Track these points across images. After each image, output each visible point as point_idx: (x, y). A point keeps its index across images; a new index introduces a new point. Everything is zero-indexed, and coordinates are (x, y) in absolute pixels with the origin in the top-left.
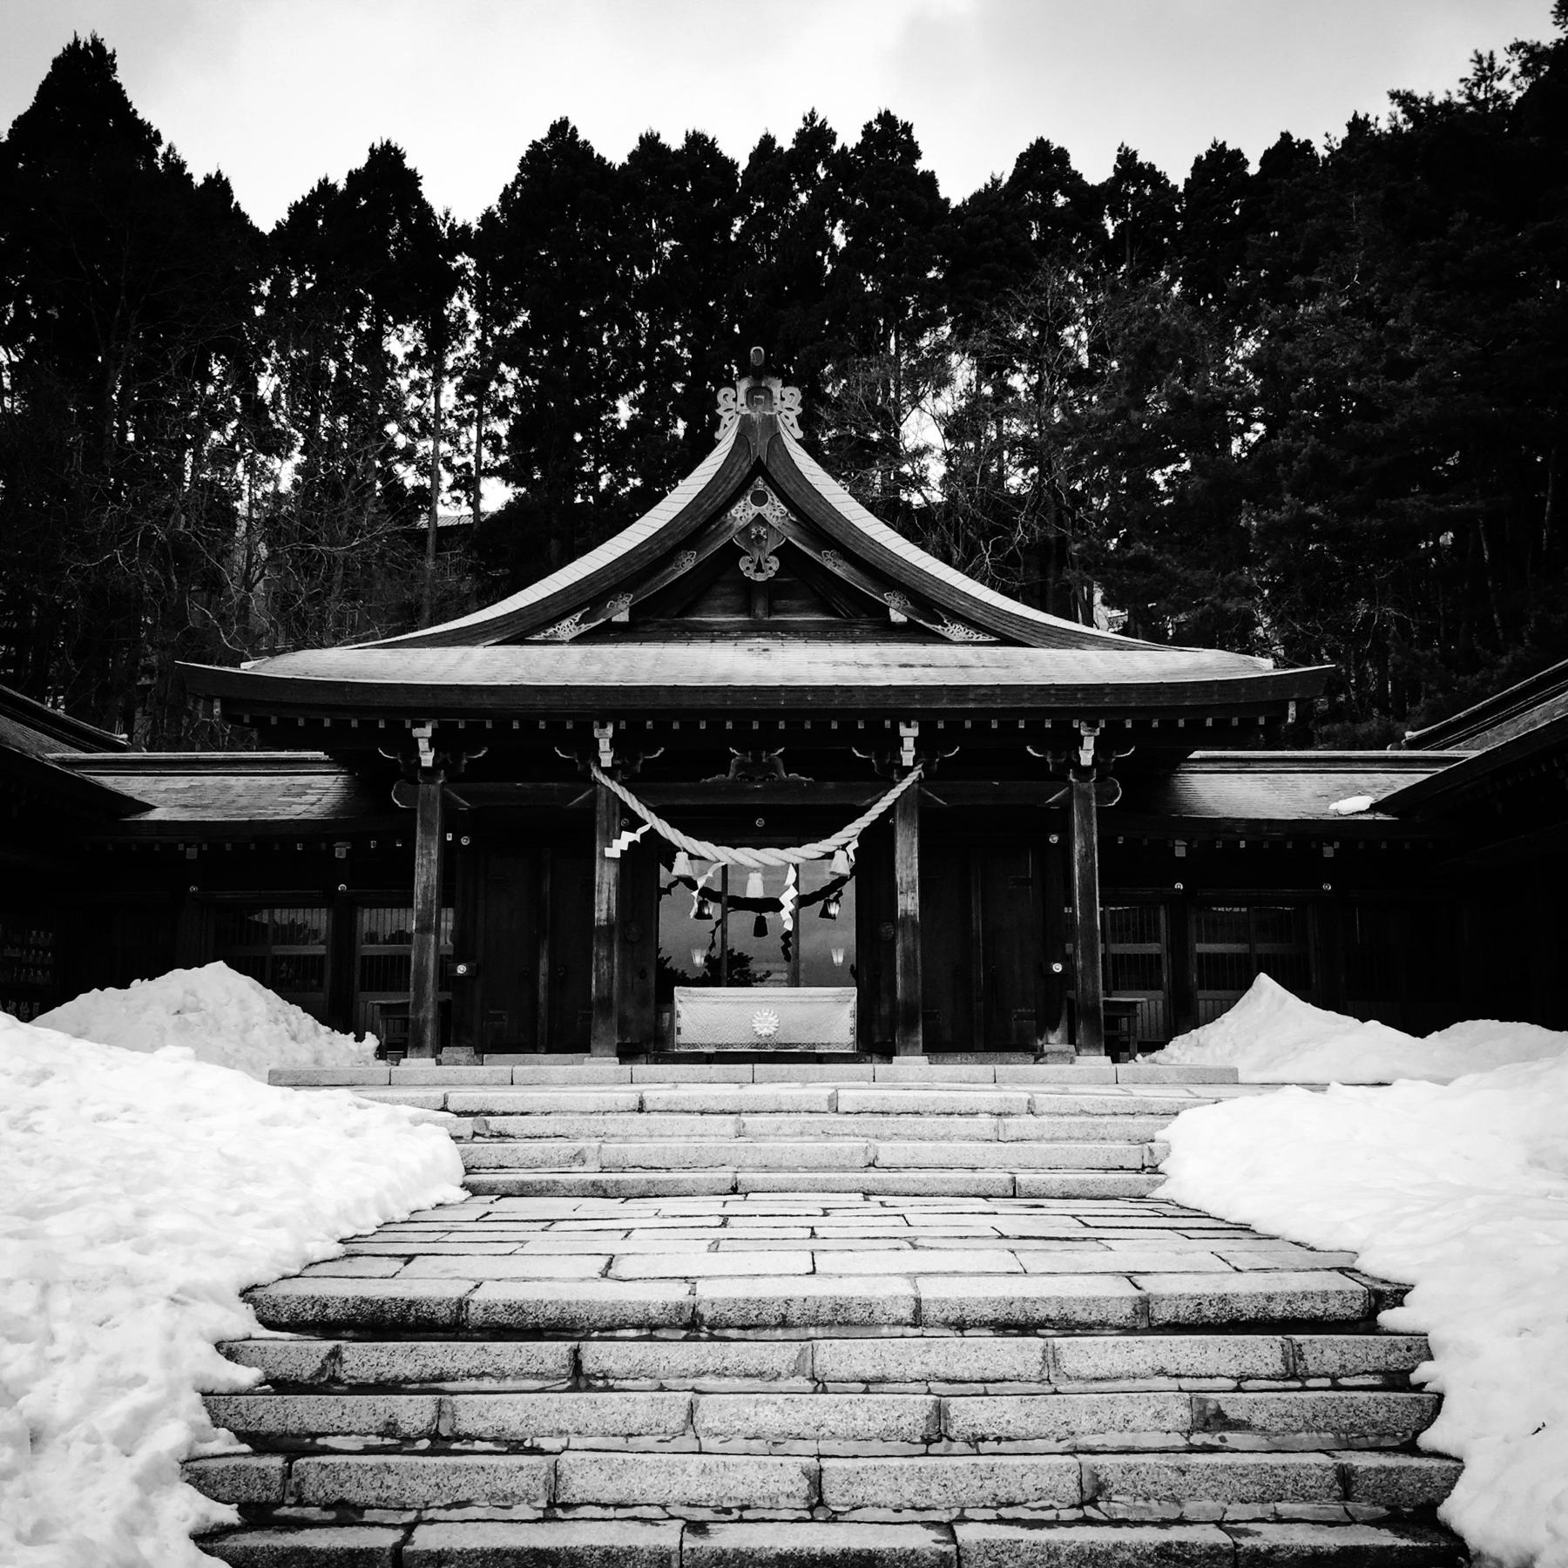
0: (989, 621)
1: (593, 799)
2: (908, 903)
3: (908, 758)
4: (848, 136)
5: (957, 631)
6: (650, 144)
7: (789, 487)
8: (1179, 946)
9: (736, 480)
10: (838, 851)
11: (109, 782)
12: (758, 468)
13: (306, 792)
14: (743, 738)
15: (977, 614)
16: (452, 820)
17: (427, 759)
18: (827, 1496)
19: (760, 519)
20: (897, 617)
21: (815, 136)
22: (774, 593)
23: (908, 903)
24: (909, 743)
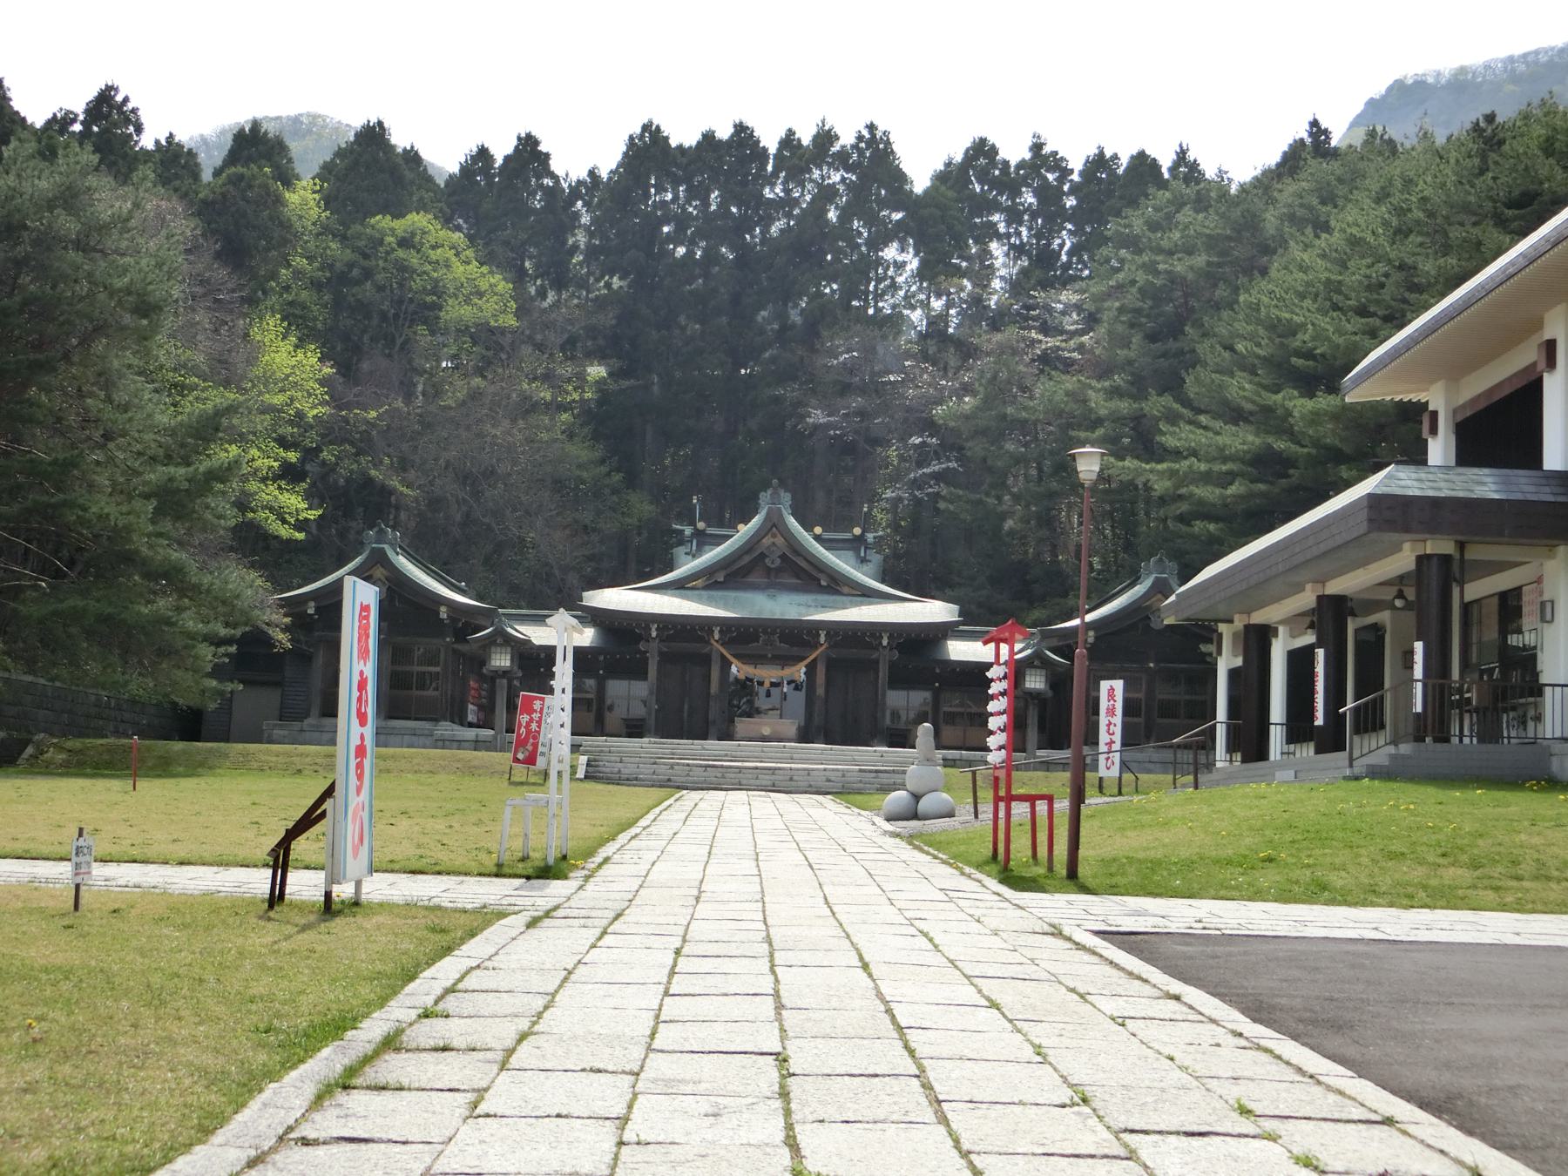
2: (820, 691)
3: (822, 640)
4: (847, 138)
5: (846, 590)
6: (708, 137)
12: (774, 525)
14: (765, 632)
17: (654, 634)
18: (784, 1001)
21: (825, 137)
22: (779, 570)
23: (820, 691)
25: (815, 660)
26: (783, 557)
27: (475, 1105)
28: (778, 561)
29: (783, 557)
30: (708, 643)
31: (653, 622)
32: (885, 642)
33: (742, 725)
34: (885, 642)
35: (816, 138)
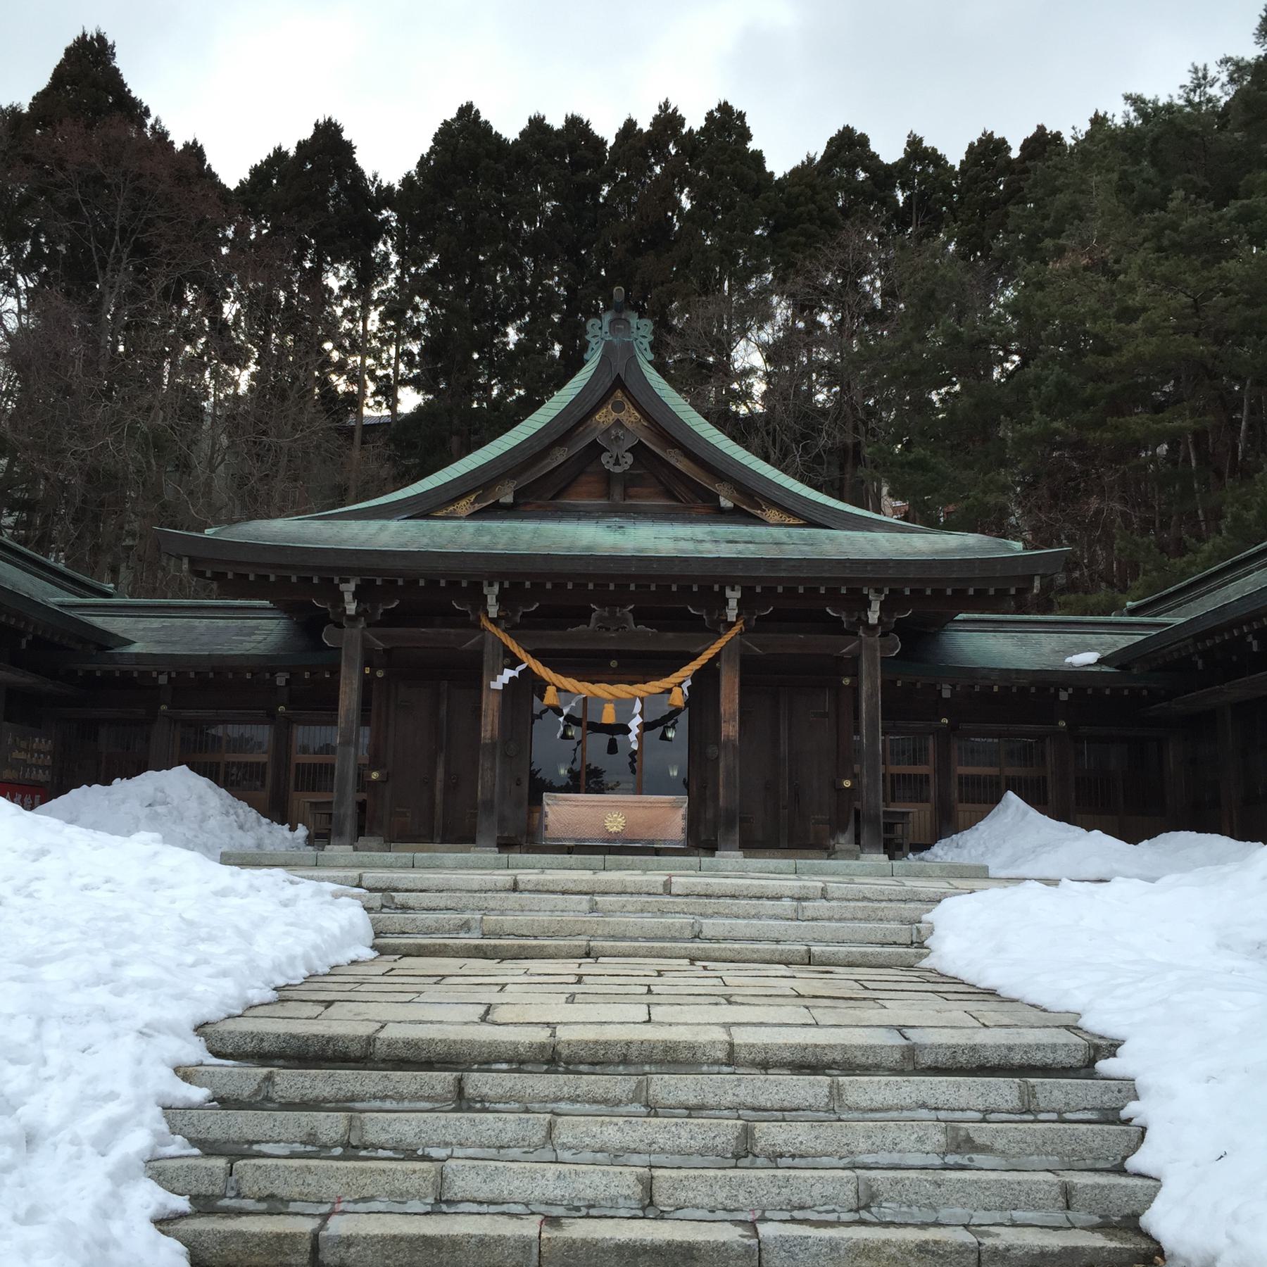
0: (797, 508)
1: (482, 643)
2: (730, 729)
3: (732, 615)
4: (695, 121)
5: (773, 515)
7: (642, 399)
8: (944, 768)
9: (600, 392)
10: (677, 687)
11: (98, 622)
12: (618, 385)
13: (255, 632)
15: (788, 503)
16: (369, 659)
17: (351, 608)
18: (657, 1198)
19: (618, 423)
20: (725, 503)
22: (629, 482)
23: (730, 729)
24: (733, 603)
25: (717, 657)
26: (639, 450)
27: (487, 1012)
28: (629, 459)
29: (639, 450)
30: (476, 626)
31: (345, 574)
32: (873, 617)
33: (565, 812)
34: (873, 617)
35: (657, 121)
